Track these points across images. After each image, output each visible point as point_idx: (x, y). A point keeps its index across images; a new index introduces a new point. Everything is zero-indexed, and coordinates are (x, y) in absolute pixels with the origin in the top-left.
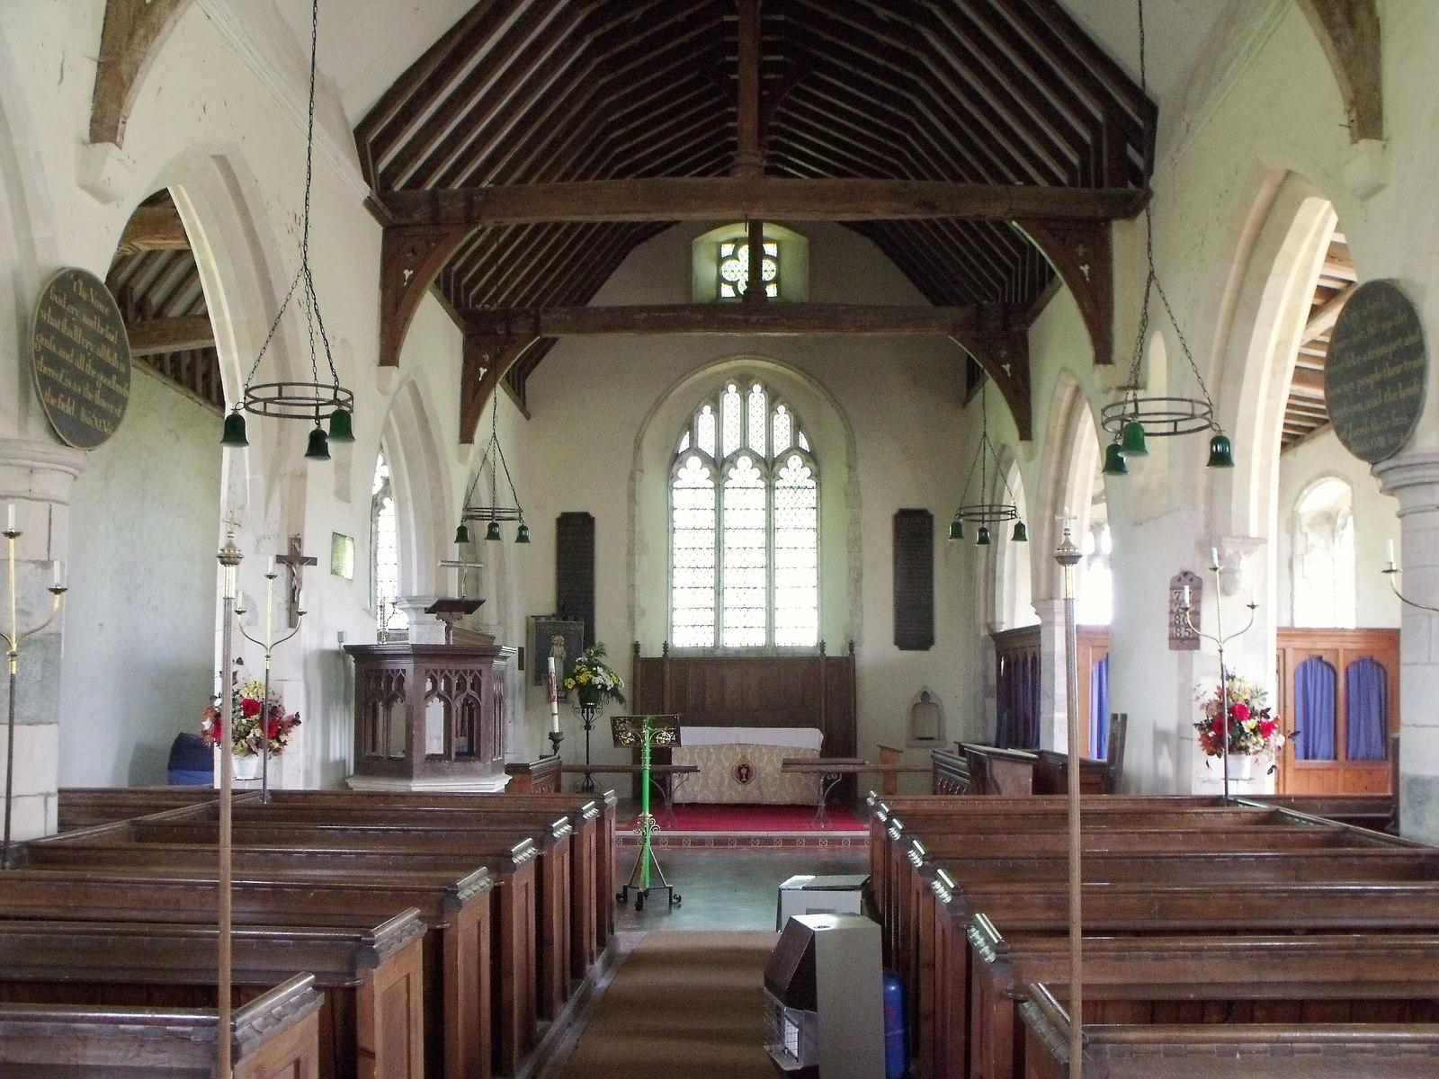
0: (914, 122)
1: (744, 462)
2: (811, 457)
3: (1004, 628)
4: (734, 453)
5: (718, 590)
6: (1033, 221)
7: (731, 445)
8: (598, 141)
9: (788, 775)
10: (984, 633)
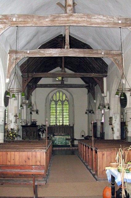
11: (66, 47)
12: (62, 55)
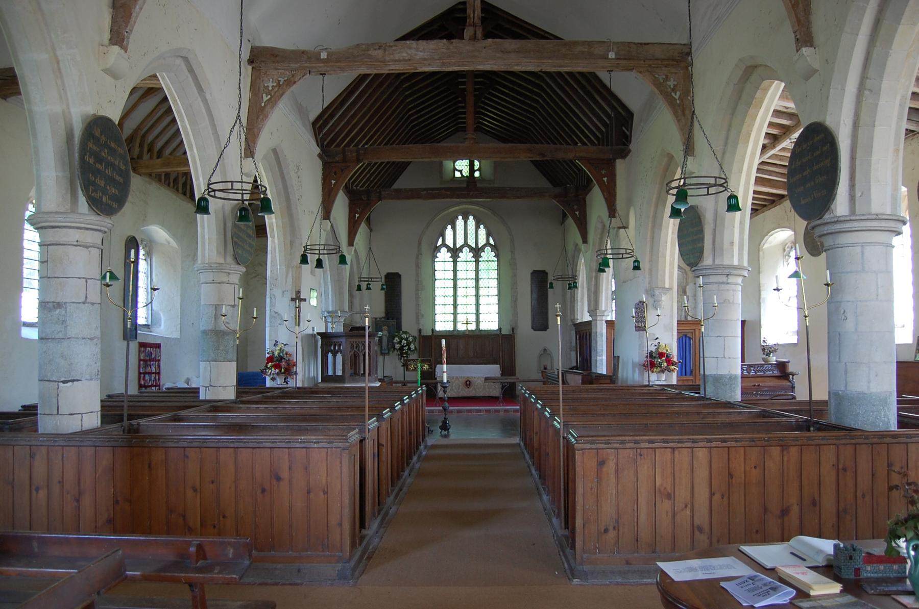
0: (538, 107)
1: (466, 250)
2: (494, 248)
3: (579, 321)
4: (461, 246)
5: (455, 306)
6: (587, 161)
7: (460, 242)
8: (404, 116)
9: (487, 384)
10: (570, 323)
11: (468, 32)
12: (454, 65)
